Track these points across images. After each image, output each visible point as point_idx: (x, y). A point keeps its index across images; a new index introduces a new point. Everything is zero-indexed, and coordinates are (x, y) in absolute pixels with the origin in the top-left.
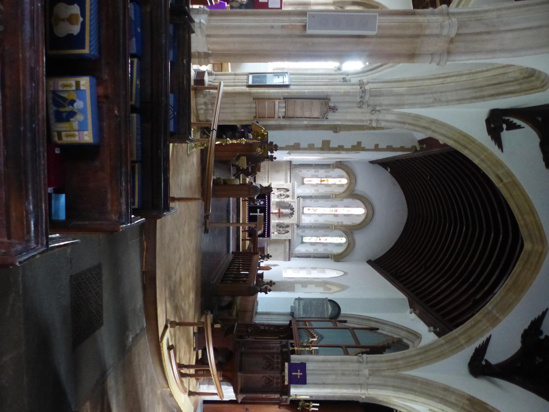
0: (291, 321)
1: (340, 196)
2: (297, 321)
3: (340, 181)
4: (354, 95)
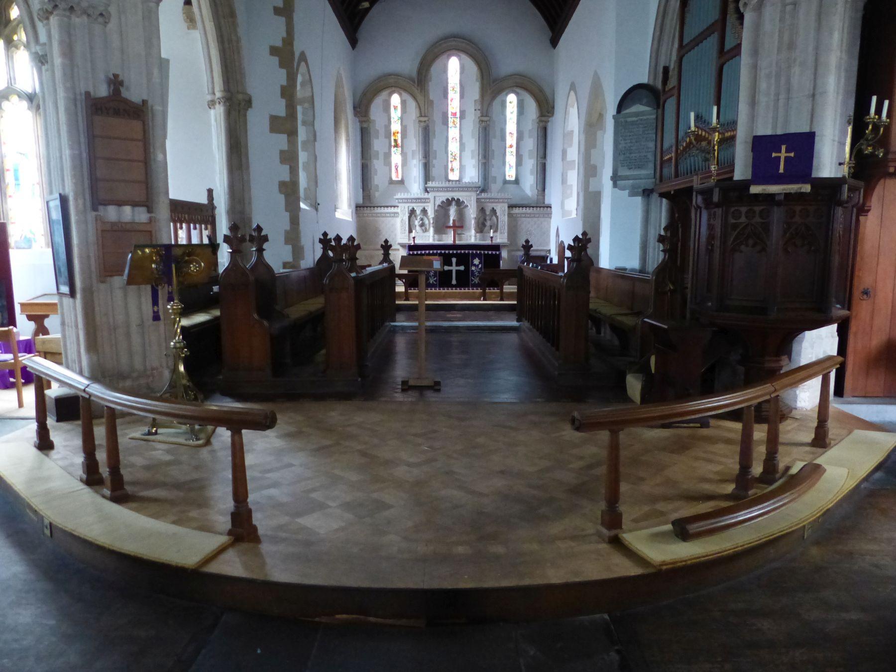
0: (662, 195)
1: (422, 105)
2: (661, 180)
3: (395, 108)
4: (68, 32)
